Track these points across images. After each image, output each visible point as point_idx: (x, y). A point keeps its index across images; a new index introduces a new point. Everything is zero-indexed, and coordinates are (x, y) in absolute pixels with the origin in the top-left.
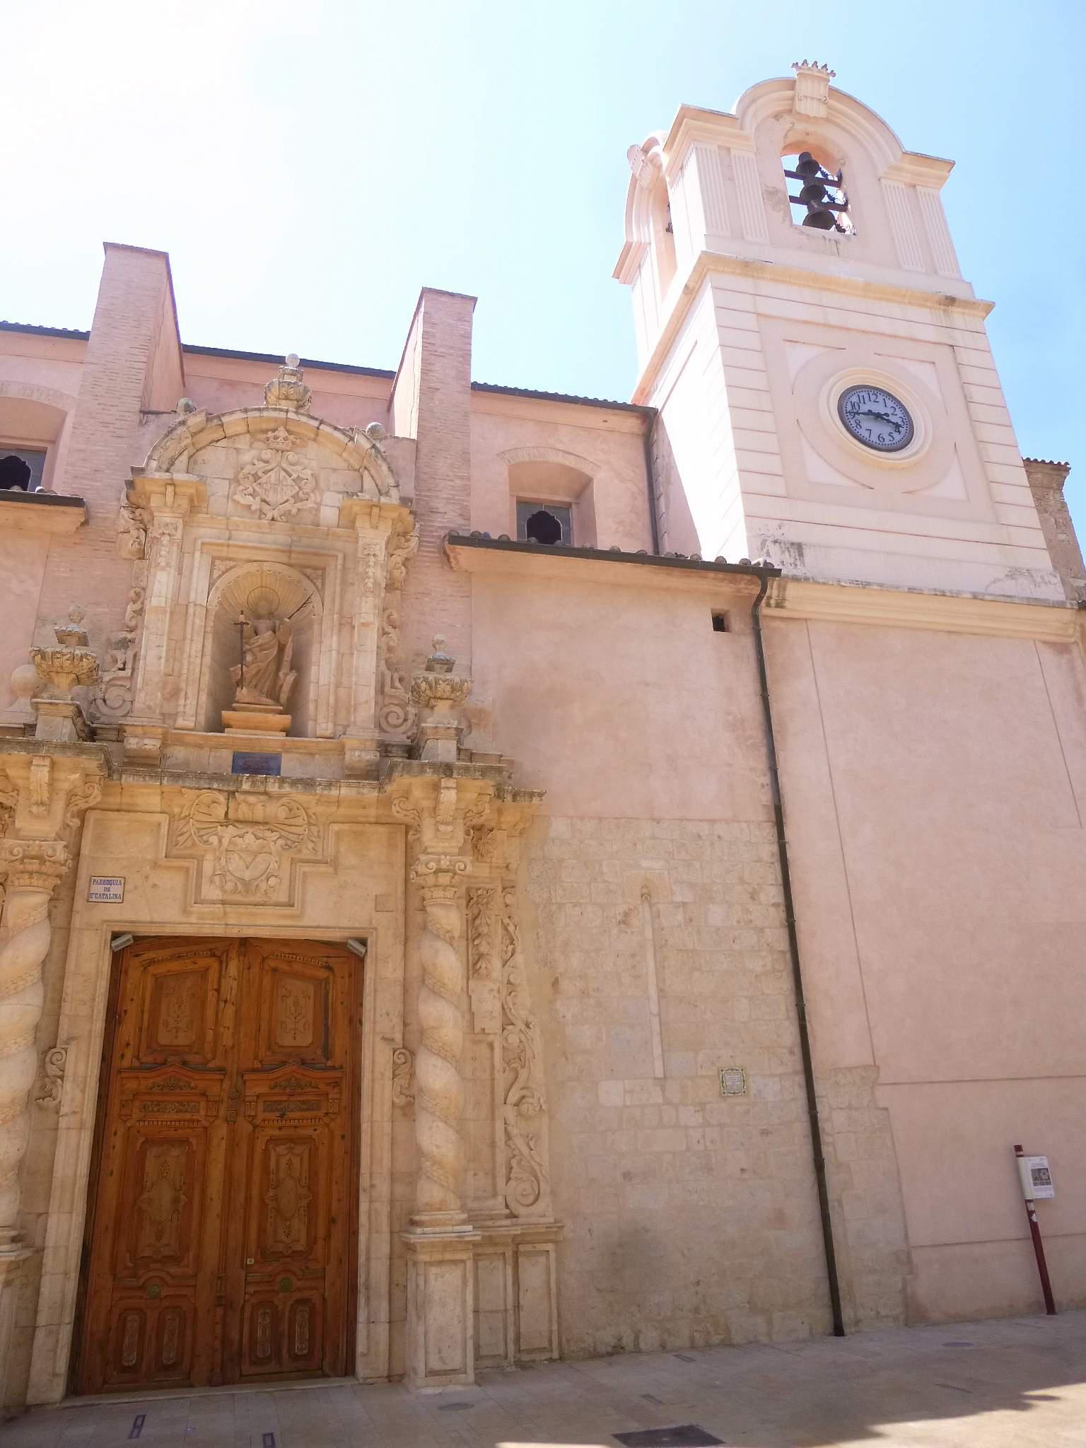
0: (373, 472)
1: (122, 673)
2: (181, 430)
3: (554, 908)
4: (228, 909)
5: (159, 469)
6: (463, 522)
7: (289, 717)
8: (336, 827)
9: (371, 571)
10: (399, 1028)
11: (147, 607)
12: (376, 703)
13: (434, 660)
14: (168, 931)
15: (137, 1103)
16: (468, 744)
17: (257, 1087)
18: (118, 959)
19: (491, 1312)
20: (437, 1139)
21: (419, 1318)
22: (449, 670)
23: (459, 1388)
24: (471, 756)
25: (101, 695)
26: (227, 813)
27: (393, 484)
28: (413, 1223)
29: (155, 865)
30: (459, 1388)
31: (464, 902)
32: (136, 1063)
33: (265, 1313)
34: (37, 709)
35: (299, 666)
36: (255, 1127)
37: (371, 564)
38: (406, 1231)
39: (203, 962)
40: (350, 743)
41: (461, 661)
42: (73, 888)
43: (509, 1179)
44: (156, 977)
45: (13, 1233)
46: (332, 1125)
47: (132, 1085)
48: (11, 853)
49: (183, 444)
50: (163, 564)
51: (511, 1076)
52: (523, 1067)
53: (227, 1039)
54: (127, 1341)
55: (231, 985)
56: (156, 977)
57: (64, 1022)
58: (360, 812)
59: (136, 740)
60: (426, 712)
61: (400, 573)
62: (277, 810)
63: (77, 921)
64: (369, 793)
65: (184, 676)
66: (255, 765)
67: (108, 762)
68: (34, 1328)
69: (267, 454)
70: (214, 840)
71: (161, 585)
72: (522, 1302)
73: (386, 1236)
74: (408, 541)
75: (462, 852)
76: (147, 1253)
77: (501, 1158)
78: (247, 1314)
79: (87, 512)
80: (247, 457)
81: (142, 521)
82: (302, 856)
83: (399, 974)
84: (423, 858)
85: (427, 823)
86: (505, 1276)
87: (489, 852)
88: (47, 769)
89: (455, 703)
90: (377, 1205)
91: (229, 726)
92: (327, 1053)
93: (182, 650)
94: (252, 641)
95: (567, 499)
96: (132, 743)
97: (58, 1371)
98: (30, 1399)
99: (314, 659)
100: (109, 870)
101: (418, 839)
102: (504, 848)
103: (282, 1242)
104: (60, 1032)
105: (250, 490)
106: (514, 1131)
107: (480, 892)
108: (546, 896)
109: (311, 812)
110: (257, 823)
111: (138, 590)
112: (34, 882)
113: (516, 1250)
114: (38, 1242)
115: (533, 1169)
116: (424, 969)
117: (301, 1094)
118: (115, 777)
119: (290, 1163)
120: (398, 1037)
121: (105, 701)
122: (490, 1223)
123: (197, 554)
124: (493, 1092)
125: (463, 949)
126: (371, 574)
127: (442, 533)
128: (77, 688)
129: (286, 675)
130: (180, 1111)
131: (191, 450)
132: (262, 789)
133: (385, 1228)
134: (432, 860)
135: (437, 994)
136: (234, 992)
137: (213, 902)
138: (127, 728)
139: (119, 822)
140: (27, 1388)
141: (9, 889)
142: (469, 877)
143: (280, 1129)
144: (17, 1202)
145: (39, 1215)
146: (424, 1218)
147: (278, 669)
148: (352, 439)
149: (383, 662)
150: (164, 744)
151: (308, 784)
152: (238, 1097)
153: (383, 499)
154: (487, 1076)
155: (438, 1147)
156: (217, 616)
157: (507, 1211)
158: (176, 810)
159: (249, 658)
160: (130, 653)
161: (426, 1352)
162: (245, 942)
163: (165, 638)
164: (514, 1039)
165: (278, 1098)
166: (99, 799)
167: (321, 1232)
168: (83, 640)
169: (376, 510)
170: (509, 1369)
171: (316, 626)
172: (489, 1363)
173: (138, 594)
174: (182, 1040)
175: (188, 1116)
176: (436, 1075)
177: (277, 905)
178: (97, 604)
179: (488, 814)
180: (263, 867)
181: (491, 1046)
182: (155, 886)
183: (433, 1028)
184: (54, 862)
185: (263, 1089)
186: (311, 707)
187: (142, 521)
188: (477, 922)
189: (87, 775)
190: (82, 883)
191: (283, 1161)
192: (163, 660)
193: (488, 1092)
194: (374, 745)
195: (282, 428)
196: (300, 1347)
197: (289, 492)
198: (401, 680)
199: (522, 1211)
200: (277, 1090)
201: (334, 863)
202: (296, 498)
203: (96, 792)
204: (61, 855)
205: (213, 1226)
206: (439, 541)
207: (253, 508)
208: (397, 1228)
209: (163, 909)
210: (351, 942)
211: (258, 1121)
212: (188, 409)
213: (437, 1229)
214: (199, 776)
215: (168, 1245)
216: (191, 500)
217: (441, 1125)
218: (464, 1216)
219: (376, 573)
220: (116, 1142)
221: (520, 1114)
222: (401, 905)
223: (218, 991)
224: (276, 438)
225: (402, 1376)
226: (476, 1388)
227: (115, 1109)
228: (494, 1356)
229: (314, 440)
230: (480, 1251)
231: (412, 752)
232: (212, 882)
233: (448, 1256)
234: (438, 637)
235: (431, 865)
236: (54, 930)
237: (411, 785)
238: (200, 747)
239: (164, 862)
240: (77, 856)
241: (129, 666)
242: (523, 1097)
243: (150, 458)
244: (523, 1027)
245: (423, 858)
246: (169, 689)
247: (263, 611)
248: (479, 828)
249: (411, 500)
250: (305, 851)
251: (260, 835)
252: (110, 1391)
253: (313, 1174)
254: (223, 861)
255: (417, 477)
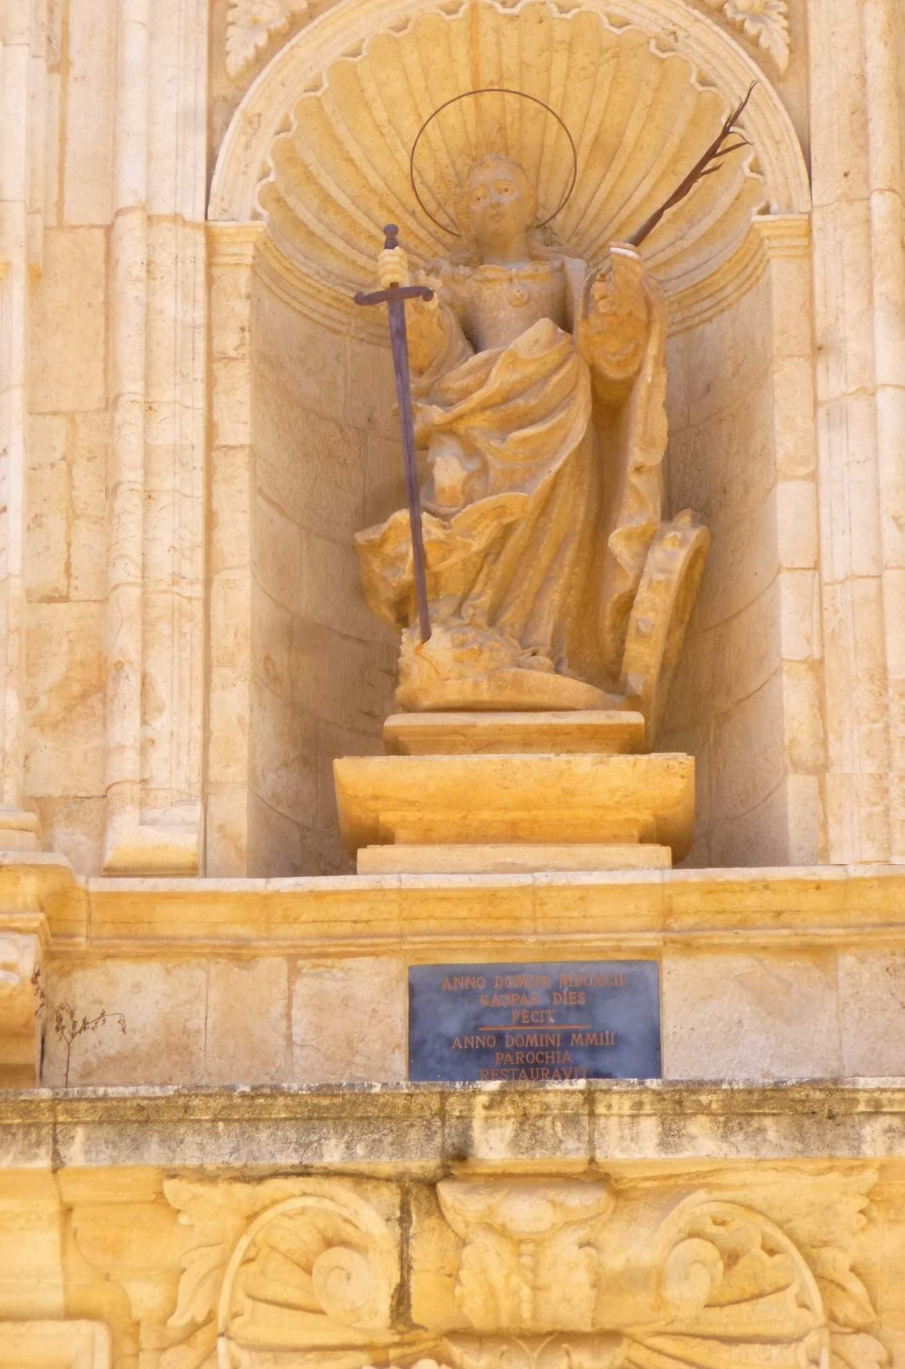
7: (682, 762)
26: (401, 1297)
35: (703, 489)
66: (528, 1030)
91: (383, 837)
94: (455, 380)
109: (838, 1261)
129: (648, 541)
132: (573, 1154)
150: (58, 956)
151: (815, 1109)
158: (145, 1297)
159: (448, 470)
186: (792, 701)
214: (250, 1107)
238: (239, 954)
246: (55, 670)
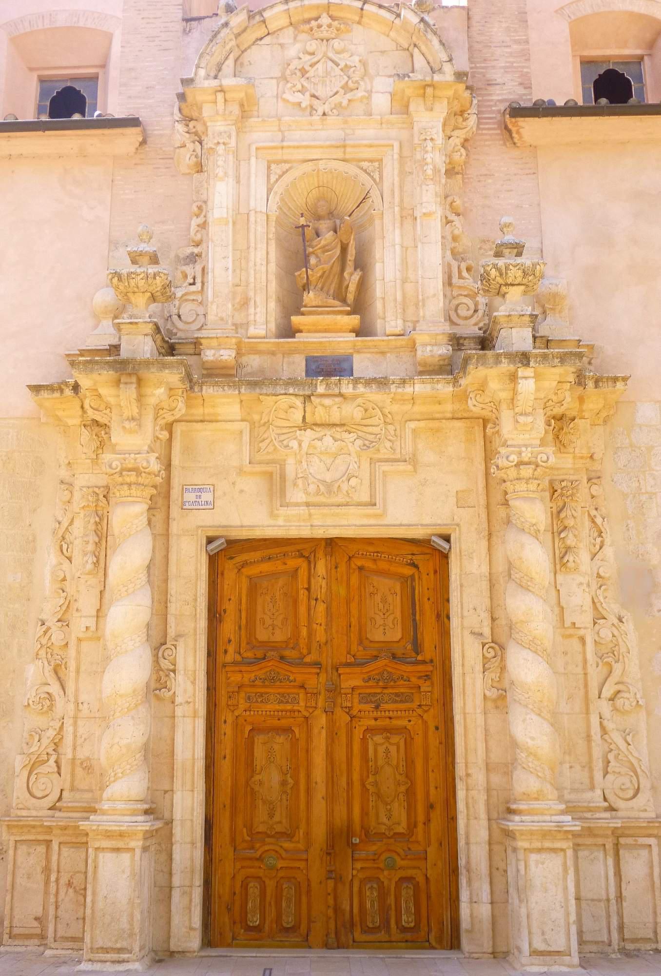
0: (423, 48)
1: (193, 288)
2: (225, 32)
3: (644, 498)
4: (313, 510)
5: (208, 77)
6: (523, 91)
7: (358, 317)
8: (412, 425)
9: (429, 157)
10: (487, 622)
11: (210, 220)
12: (445, 296)
13: (502, 245)
14: (258, 534)
15: (242, 695)
16: (543, 330)
17: (351, 680)
18: (213, 560)
19: (593, 900)
20: (531, 731)
21: (521, 901)
22: (519, 254)
23: (565, 969)
24: (548, 343)
25: (175, 311)
26: (304, 417)
27: (446, 58)
28: (510, 811)
29: (240, 471)
30: (565, 969)
31: (547, 494)
32: (238, 658)
33: (372, 888)
34: (119, 330)
35: (362, 264)
36: (352, 717)
37: (429, 148)
38: (505, 819)
39: (292, 563)
40: (420, 338)
41: (531, 244)
42: (168, 496)
43: (606, 773)
44: (250, 578)
45: (146, 806)
46: (425, 716)
47: (236, 678)
48: (110, 466)
49: (228, 47)
50: (221, 174)
51: (605, 670)
52: (617, 661)
53: (320, 635)
54: (250, 905)
55: (320, 584)
56: (250, 578)
57: (171, 620)
58: (437, 408)
59: (213, 351)
60: (499, 299)
61: (460, 156)
62: (351, 411)
63: (174, 528)
64: (444, 388)
65: (252, 285)
66: (328, 368)
67: (189, 377)
68: (171, 888)
69: (312, 46)
70: (294, 444)
71: (221, 196)
72: (624, 893)
73: (484, 823)
74: (465, 120)
75: (543, 443)
76: (261, 828)
77: (597, 752)
78: (356, 889)
79: (144, 131)
80: (293, 51)
81: (196, 134)
82: (380, 456)
83: (485, 569)
84: (503, 451)
85: (506, 417)
86: (606, 865)
87: (571, 442)
88: (134, 386)
89: (528, 288)
90: (473, 793)
91: (301, 331)
92: (417, 647)
93: (247, 260)
94: (314, 243)
95: (639, 52)
96: (209, 355)
97: (194, 926)
98: (173, 948)
99: (378, 256)
100: (199, 479)
101: (498, 432)
102: (586, 437)
103: (384, 824)
104: (169, 630)
105: (299, 87)
106: (609, 725)
107: (564, 484)
108: (636, 484)
109: (386, 411)
110: (334, 425)
111: (199, 203)
112: (134, 492)
113: (617, 842)
114: (167, 815)
115: (632, 765)
116: (510, 563)
117: (392, 687)
118: (196, 389)
119: (387, 751)
120: (487, 631)
121: (179, 316)
122: (588, 815)
123: (253, 160)
124: (586, 685)
125: (550, 544)
126: (429, 160)
127: (502, 107)
128: (153, 307)
129: (351, 274)
130: (282, 702)
131: (237, 52)
132: (337, 391)
133: (483, 815)
134: (512, 453)
135: (525, 588)
136: (323, 591)
137: (297, 505)
138: (203, 341)
139: (204, 432)
140: (169, 938)
141: (112, 501)
142: (552, 468)
143: (376, 719)
144: (147, 780)
145: (166, 792)
146: (522, 806)
147: (343, 270)
148: (398, 15)
149: (449, 253)
150: (239, 354)
151: (382, 383)
152: (334, 690)
153: (437, 77)
154: (579, 670)
155: (533, 739)
156: (278, 222)
157: (606, 804)
158: (256, 417)
159: (313, 261)
160: (198, 267)
161: (530, 933)
162: (331, 543)
163: (230, 247)
164: (606, 633)
165: (373, 691)
166: (183, 411)
167: (421, 818)
168: (154, 259)
169: (429, 90)
170: (613, 956)
171: (377, 222)
172: (594, 948)
173: (200, 208)
174: (279, 636)
175: (289, 707)
176: (527, 669)
177: (359, 504)
178: (163, 222)
179: (569, 404)
180: (343, 468)
181: (582, 640)
182: (242, 491)
183: (522, 621)
184: (149, 474)
185: (358, 682)
186: (379, 305)
187: (196, 134)
188: (562, 515)
189: (171, 389)
190: (175, 492)
191: (381, 750)
192: (230, 271)
193: (582, 687)
194: (445, 339)
195: (325, 15)
196: (407, 920)
197: (337, 85)
198: (468, 269)
199: (620, 804)
200: (371, 683)
201: (413, 461)
202: (346, 89)
203: (180, 403)
204: (155, 466)
205: (319, 808)
206: (499, 117)
207: (303, 105)
208: (495, 815)
209: (251, 515)
210: (433, 538)
211: (354, 712)
212: (230, 9)
213: (536, 818)
215: (280, 822)
216: (242, 105)
217: (535, 717)
218: (563, 807)
219: (436, 159)
220: (226, 730)
221: (615, 709)
222: (483, 501)
223: (308, 589)
224: (319, 26)
225: (506, 954)
226: (581, 970)
227: (223, 700)
228: (596, 943)
229: (359, 23)
230: (580, 841)
231: (485, 343)
232: (295, 484)
233: (547, 844)
234: (506, 219)
235: (511, 458)
236: (154, 536)
237: (487, 375)
239: (248, 468)
240: (168, 466)
241: (199, 281)
242: (619, 692)
243: (198, 67)
244: (616, 621)
245: (503, 451)
247: (323, 211)
248: (560, 418)
249: (466, 74)
250: (383, 451)
251: (338, 436)
252: (237, 946)
253: (410, 763)
254: (304, 464)
255: (470, 48)
